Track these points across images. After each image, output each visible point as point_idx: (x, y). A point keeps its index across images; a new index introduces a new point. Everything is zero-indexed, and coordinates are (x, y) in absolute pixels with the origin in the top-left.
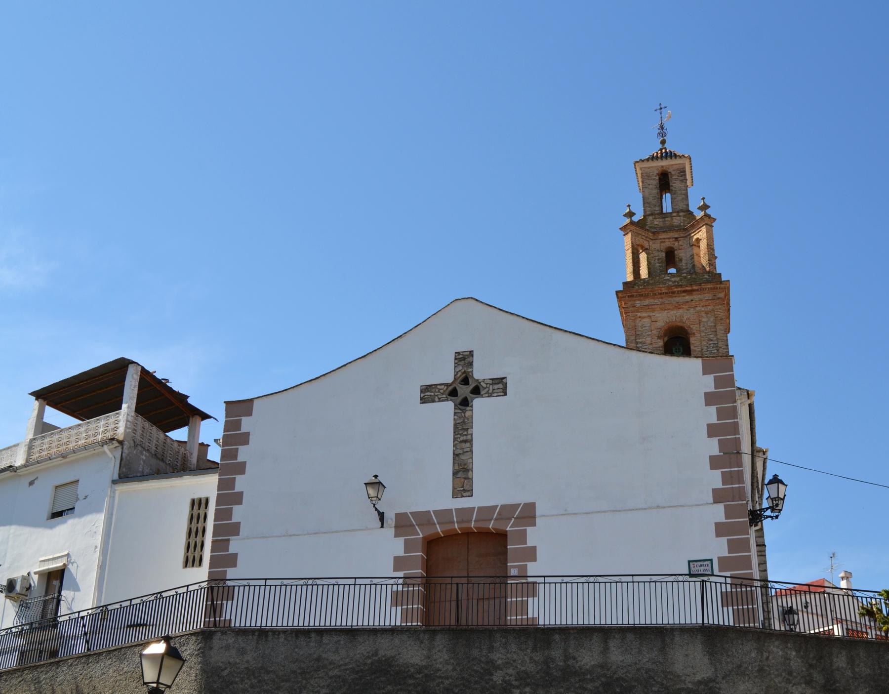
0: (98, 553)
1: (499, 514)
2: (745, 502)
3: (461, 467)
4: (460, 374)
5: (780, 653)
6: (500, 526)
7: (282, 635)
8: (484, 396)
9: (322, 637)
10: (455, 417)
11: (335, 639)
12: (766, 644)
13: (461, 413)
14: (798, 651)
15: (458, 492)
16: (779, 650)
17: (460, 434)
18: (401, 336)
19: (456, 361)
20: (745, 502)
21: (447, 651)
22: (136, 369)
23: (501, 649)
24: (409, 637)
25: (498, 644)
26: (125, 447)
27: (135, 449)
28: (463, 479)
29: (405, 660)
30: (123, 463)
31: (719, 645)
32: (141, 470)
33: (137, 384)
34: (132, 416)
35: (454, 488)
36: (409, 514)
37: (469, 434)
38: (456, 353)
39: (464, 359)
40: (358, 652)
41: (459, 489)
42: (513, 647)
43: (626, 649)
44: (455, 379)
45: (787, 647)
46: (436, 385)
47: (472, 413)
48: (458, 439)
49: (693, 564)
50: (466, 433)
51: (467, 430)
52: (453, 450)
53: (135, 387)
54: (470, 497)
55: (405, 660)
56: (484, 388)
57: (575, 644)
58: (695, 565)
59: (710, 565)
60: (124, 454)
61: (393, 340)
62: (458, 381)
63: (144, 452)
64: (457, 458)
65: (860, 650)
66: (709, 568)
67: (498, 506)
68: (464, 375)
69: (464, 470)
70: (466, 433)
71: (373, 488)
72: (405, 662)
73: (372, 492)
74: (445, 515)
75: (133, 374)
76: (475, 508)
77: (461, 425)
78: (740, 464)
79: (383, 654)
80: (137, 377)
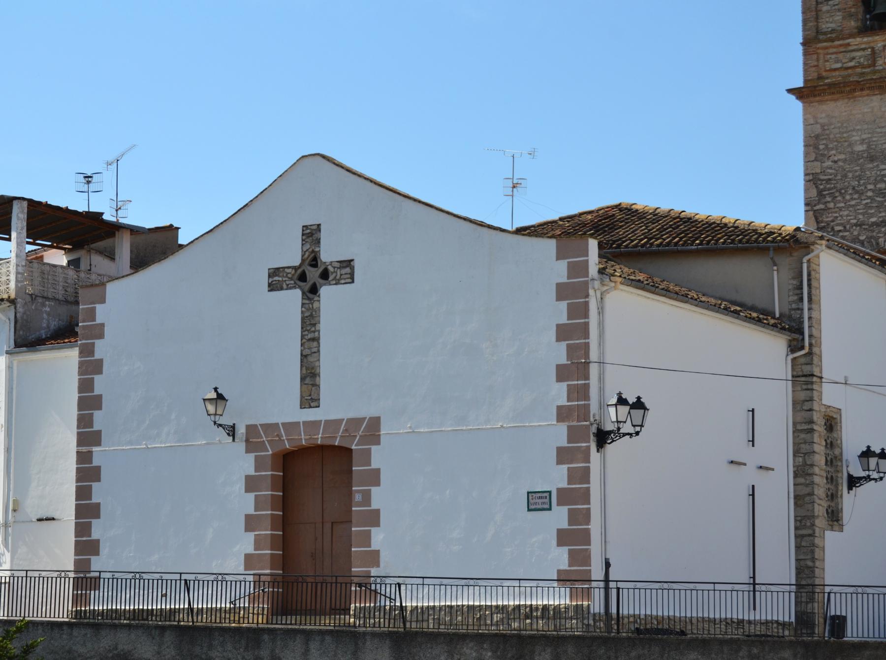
0: (3, 432)
1: (346, 430)
2: (587, 423)
3: (309, 372)
4: (307, 254)
5: (474, 654)
6: (345, 444)
7: (40, 627)
8: (332, 283)
9: (72, 630)
10: (303, 309)
11: (83, 632)
12: (458, 646)
13: (309, 303)
14: (494, 652)
15: (305, 401)
16: (473, 651)
17: (308, 331)
18: (247, 204)
19: (304, 237)
20: (587, 423)
21: (174, 647)
22: (21, 206)
23: (218, 647)
24: (144, 633)
25: (216, 642)
26: (18, 306)
27: (33, 303)
28: (311, 386)
29: (139, 654)
30: (18, 325)
31: (405, 650)
32: (45, 325)
33: (25, 224)
34: (23, 266)
35: (302, 397)
36: (259, 426)
37: (317, 331)
38: (303, 226)
39: (311, 234)
40: (102, 645)
41: (306, 398)
42: (229, 646)
43: (324, 651)
44: (303, 261)
45: (482, 648)
46: (284, 268)
47: (320, 303)
48: (306, 337)
49: (532, 496)
50: (313, 329)
51: (314, 325)
52: (301, 350)
53: (22, 229)
54: (317, 408)
55: (139, 654)
56: (332, 273)
57: (281, 644)
58: (534, 497)
59: (548, 497)
60: (18, 315)
61: (239, 210)
62: (307, 262)
63: (47, 303)
64: (305, 359)
65: (569, 646)
66: (547, 500)
67: (344, 419)
68: (313, 255)
69: (311, 375)
70: (313, 329)
71: (210, 404)
72: (139, 656)
73: (211, 408)
74: (291, 427)
75: (18, 214)
76: (321, 421)
77: (308, 320)
78: (587, 377)
79: (122, 649)
80: (24, 216)
